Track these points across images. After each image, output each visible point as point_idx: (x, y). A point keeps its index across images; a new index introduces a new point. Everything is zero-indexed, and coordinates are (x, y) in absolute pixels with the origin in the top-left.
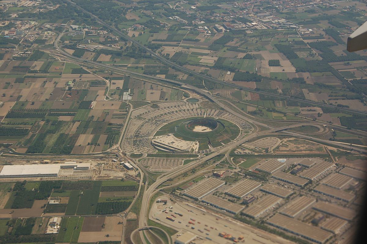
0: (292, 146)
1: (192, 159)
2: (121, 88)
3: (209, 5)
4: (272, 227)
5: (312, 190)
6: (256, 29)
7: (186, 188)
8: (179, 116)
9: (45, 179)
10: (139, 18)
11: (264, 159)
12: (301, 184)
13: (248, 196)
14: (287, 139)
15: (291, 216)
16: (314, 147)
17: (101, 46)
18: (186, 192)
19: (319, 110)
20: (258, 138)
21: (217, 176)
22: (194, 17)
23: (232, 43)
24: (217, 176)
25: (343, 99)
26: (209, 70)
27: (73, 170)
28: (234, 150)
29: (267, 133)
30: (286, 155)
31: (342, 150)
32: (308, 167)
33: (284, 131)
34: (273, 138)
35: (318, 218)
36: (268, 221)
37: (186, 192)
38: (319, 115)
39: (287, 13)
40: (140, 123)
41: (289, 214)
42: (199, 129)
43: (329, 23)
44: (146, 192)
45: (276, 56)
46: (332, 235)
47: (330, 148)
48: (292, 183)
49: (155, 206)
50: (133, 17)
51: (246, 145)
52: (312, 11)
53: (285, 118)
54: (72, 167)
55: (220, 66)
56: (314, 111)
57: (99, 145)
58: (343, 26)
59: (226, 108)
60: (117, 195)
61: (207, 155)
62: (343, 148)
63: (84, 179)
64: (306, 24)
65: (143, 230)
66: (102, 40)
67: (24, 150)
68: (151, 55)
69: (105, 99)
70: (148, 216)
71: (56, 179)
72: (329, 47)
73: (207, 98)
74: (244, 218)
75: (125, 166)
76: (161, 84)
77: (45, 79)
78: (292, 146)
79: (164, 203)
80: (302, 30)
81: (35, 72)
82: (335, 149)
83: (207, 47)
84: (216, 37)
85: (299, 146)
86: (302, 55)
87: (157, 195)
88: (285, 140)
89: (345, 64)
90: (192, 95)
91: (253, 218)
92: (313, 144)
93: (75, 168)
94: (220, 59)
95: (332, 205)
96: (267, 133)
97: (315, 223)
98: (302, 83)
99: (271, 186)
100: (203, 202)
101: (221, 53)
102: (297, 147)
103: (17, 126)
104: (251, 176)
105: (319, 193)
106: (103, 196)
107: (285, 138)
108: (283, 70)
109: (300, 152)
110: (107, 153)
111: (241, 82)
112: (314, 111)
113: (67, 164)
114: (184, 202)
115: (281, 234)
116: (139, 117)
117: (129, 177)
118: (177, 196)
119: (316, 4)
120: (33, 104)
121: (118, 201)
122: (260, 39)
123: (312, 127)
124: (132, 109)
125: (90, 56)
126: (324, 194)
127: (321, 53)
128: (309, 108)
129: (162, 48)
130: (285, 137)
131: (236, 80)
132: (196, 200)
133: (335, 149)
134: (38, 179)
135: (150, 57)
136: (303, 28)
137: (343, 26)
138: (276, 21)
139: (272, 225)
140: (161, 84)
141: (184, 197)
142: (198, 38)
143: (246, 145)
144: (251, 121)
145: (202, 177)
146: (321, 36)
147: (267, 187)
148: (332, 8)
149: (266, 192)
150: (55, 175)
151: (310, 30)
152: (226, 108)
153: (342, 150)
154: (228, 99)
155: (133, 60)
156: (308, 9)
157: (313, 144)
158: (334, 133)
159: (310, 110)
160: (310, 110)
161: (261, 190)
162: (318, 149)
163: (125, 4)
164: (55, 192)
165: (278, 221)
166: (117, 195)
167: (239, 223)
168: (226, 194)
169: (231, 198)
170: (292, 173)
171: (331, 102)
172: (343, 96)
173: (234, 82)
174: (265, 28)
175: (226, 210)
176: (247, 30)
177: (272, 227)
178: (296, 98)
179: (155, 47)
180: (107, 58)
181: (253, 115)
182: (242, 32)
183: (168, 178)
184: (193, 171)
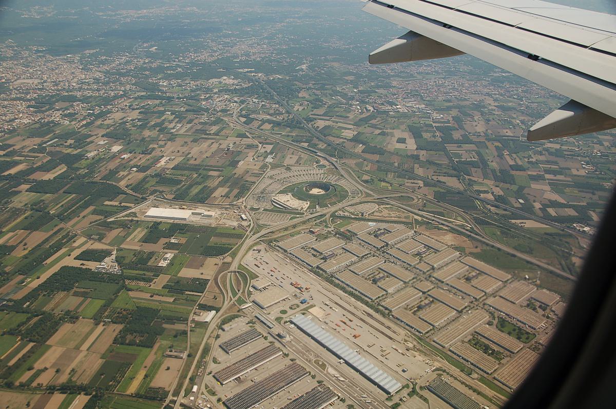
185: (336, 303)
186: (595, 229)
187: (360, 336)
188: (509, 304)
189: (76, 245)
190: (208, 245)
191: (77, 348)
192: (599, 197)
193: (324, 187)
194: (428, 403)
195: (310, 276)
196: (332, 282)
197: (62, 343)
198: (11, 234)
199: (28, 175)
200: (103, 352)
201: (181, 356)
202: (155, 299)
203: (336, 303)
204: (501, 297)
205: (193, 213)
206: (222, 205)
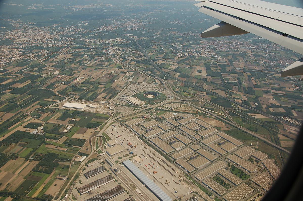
0: (183, 108)
1: (138, 109)
2: (131, 76)
3: (188, 45)
4: (151, 143)
5: (179, 129)
6: (201, 56)
7: (127, 121)
8: (147, 90)
9: (77, 110)
10: (157, 48)
11: (168, 112)
12: (175, 126)
13: (149, 128)
14: (184, 105)
15: (162, 139)
16: (193, 110)
17: (135, 58)
18: (126, 123)
19: (205, 93)
20: (172, 103)
21: (143, 117)
22: (179, 50)
23: (187, 61)
24: (143, 117)
25: (218, 90)
26: (171, 71)
27: (89, 108)
28: (158, 107)
29: (176, 101)
30: (179, 112)
31: (203, 112)
32: (184, 118)
33: (184, 101)
34: (178, 104)
35: (221, 143)
36: (151, 140)
37: (126, 123)
38: (204, 95)
39: (217, 51)
40: (128, 90)
41: (162, 139)
42: (150, 96)
43: (232, 57)
44: (110, 120)
45: (202, 68)
46: (174, 150)
47: (199, 111)
48: (172, 125)
49: (111, 126)
50: (155, 48)
51: (164, 105)
52: (228, 51)
53: (188, 95)
54: (89, 106)
55: (176, 70)
56: (203, 93)
57: (106, 98)
58: (237, 59)
59: (167, 89)
60: (99, 120)
61: (145, 108)
62: (204, 111)
63: (91, 112)
64: (222, 56)
65: (100, 136)
66: (137, 56)
67: (77, 97)
68: (151, 63)
69: (121, 80)
70: (104, 131)
71: (81, 110)
72: (226, 67)
73: (162, 83)
74: (142, 138)
75: (110, 109)
76: (147, 75)
77: (103, 70)
78: (183, 108)
79: (114, 126)
80: (220, 59)
81: (104, 66)
82: (200, 111)
83: (176, 62)
84: (183, 58)
85: (186, 108)
86: (213, 69)
87: (114, 122)
88: (182, 105)
89: (228, 75)
90: (157, 81)
91: (146, 138)
92: (193, 108)
93: (91, 107)
94: (179, 67)
95: (183, 137)
96: (176, 101)
97: (220, 144)
98: (205, 81)
99: (163, 125)
100: (130, 128)
101: (180, 65)
102: (185, 109)
103: (82, 87)
104: (158, 119)
105: (181, 130)
106: (93, 120)
107: (183, 104)
108: (201, 75)
109: (185, 111)
110: (107, 102)
111: (181, 78)
112: (203, 93)
113: (89, 105)
114: (123, 127)
115: (153, 147)
116: (129, 89)
117: (108, 113)
118: (122, 124)
119: (231, 49)
120: (94, 79)
121: (98, 123)
122: (200, 61)
123: (197, 100)
124: (129, 85)
125: (127, 62)
126: (183, 131)
127: (221, 69)
128: (201, 92)
129: (158, 61)
130: (183, 103)
131: (179, 77)
132: (128, 127)
133: (200, 111)
134: (75, 110)
135: (151, 64)
136: (221, 58)
137: (237, 59)
138: (211, 54)
139: (152, 142)
140: (147, 75)
141: (124, 125)
142: (175, 58)
143: (164, 105)
144: (173, 95)
145: (137, 117)
146: (226, 62)
147: (160, 126)
148: (237, 51)
149: (159, 127)
150: (82, 109)
151: (223, 59)
152: (167, 89)
153: (203, 112)
154: (170, 85)
155: (143, 64)
156: (227, 50)
157: (193, 108)
158: (205, 104)
159: (201, 93)
160: (201, 93)
161: (158, 126)
162: (193, 111)
163: (155, 42)
164: (77, 116)
165: (156, 142)
166: (99, 120)
167: (139, 140)
168: (142, 126)
169: (143, 128)
170: (176, 120)
171: (212, 90)
172: (219, 88)
173: (178, 78)
174: (205, 56)
175: (137, 133)
176: (197, 56)
177: (151, 143)
178: (199, 87)
179: (155, 60)
180: (133, 63)
181: (176, 93)
182: (195, 57)
183: (123, 116)
184: (135, 114)
185: (148, 155)
187: (156, 172)
188: (239, 158)
191: (14, 173)
203: (148, 155)
204: (235, 154)
205: (86, 106)
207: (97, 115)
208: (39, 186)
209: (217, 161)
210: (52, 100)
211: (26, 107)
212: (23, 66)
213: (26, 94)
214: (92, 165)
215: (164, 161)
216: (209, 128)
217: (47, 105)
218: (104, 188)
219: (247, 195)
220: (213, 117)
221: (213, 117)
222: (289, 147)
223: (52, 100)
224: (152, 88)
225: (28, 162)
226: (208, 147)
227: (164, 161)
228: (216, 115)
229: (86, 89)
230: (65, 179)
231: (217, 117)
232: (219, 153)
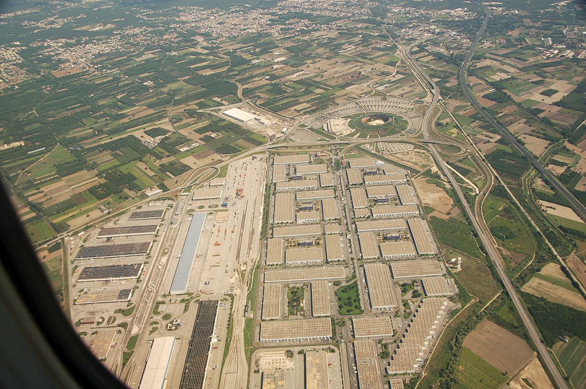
108: (543, 100)
133: (435, 169)
150: (243, 121)
185: (244, 216)
186: (19, 214)
187: (220, 245)
188: (389, 274)
189: (157, 123)
190: (230, 145)
191: (69, 186)
192: (372, 48)
193: (384, 117)
194: (184, 313)
195: (261, 187)
196: (267, 197)
197: (68, 181)
198: (139, 107)
199: (198, 70)
200: (76, 193)
201: (20, 206)
202: (147, 172)
203: (244, 216)
204: (390, 267)
205: (255, 118)
206: (285, 117)
207: (253, 137)
208: (70, 213)
209: (337, 264)
210: (222, 101)
211: (578, 233)
212: (245, 44)
213: (201, 86)
214: (156, 204)
215: (253, 233)
216: (406, 204)
217: (397, 129)
218: (116, 285)
219: (308, 338)
220: (448, 186)
221: (448, 186)
222: (537, 297)
223: (222, 101)
224: (377, 107)
225: (97, 178)
226: (358, 235)
227: (253, 233)
228: (454, 183)
229: (288, 91)
230: (106, 212)
231: (453, 190)
232: (361, 253)
